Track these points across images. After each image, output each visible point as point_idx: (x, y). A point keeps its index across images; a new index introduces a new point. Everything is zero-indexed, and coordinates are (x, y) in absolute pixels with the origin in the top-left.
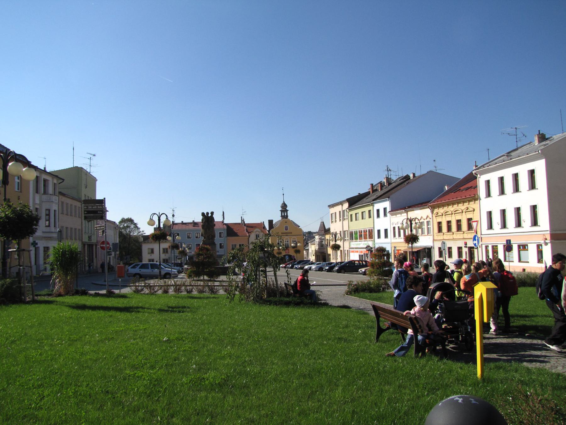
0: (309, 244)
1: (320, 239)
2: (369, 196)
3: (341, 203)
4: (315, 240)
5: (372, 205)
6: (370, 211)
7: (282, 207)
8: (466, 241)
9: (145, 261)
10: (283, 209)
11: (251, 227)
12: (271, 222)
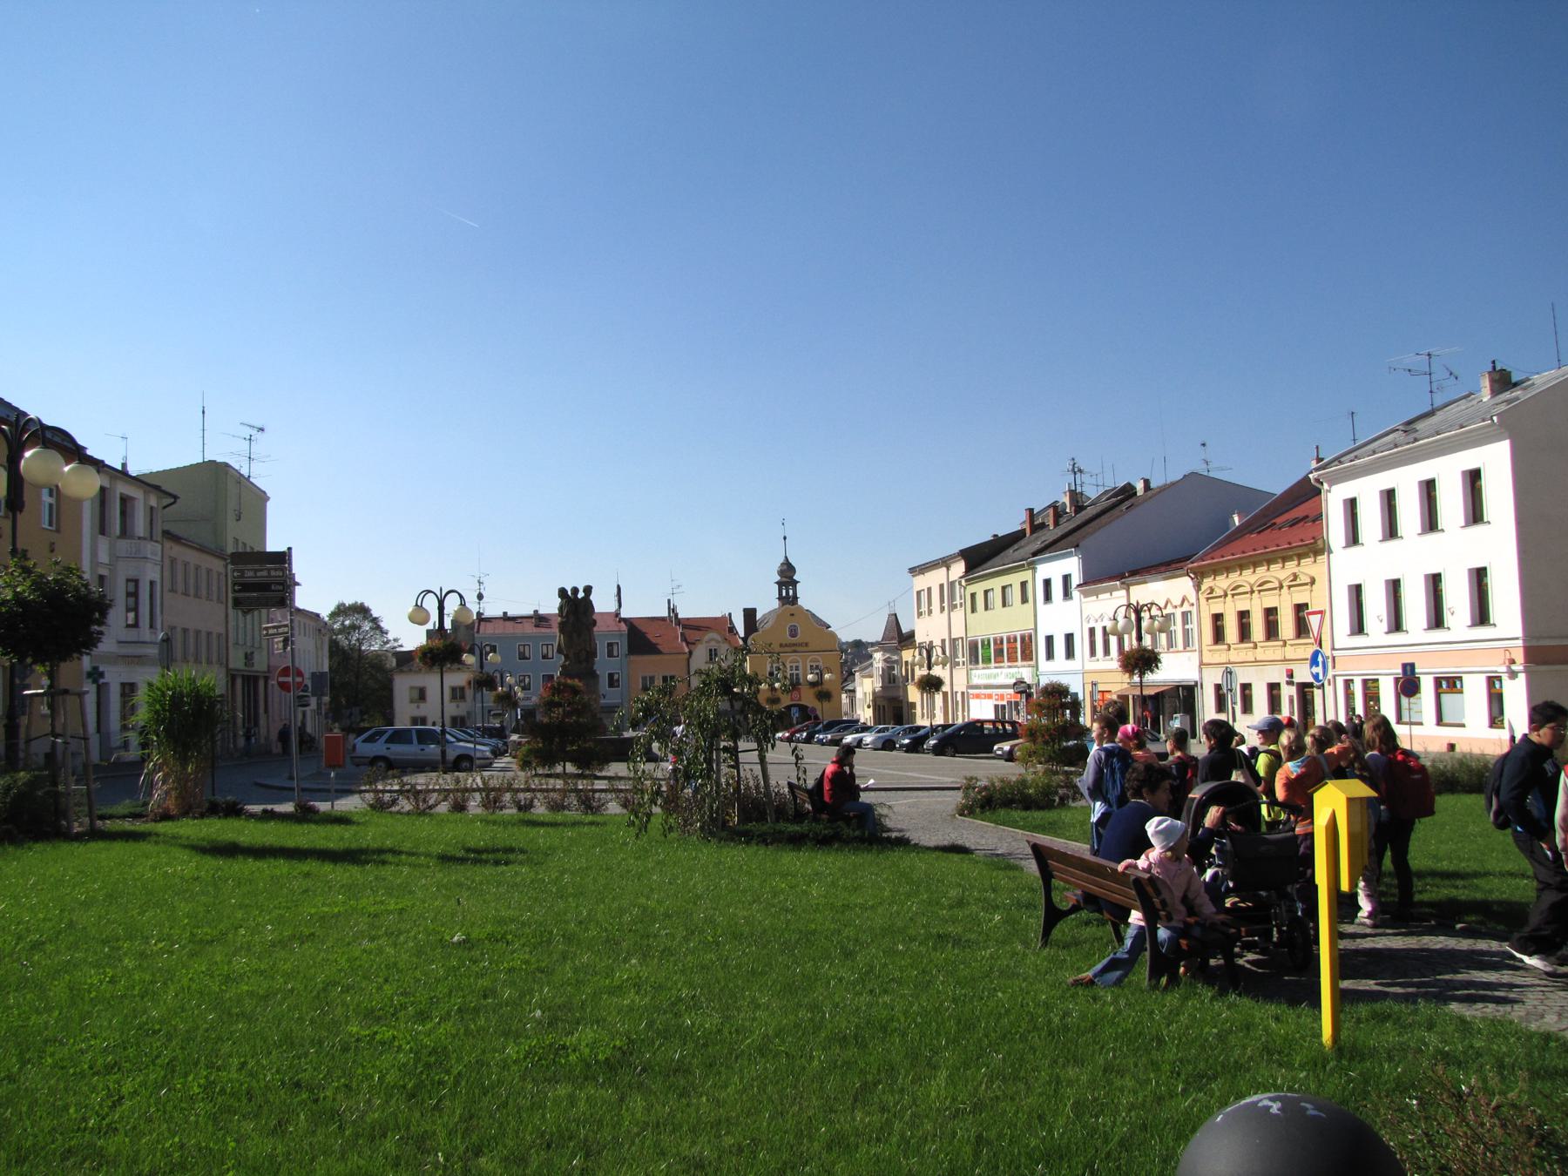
0: (857, 674)
1: (885, 660)
2: (1022, 542)
3: (945, 562)
4: (871, 665)
5: (1032, 566)
6: (1024, 584)
7: (781, 573)
8: (1290, 667)
9: (402, 722)
10: (784, 579)
11: (696, 628)
12: (750, 614)
